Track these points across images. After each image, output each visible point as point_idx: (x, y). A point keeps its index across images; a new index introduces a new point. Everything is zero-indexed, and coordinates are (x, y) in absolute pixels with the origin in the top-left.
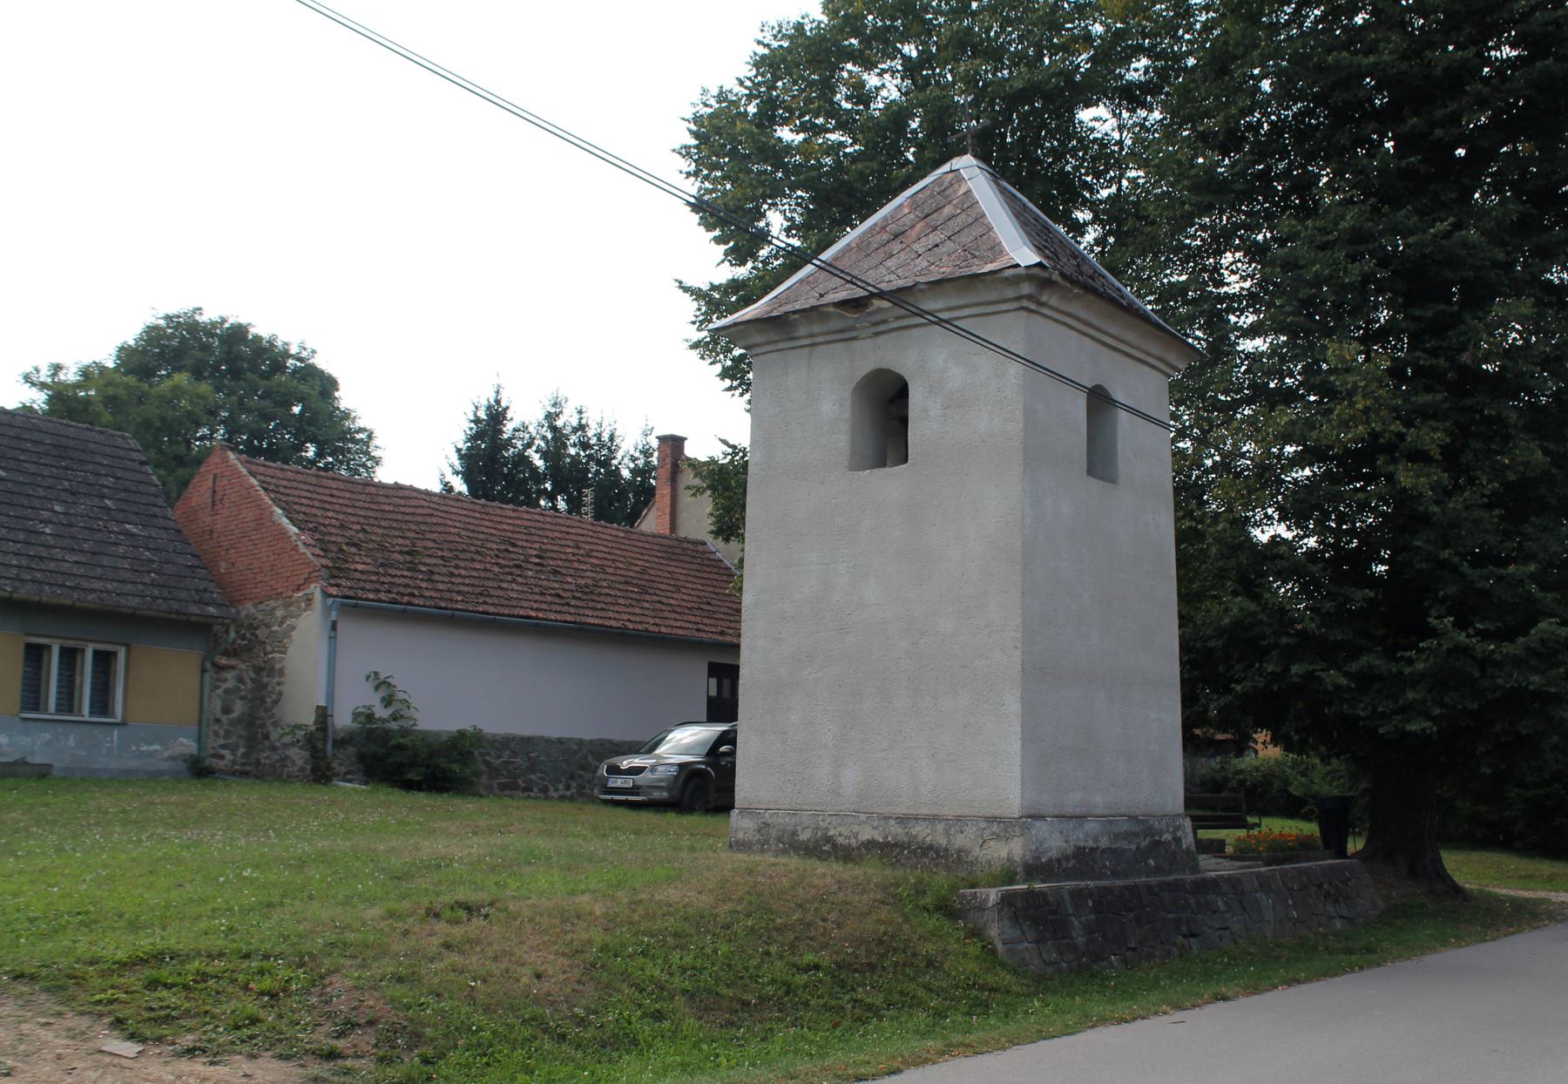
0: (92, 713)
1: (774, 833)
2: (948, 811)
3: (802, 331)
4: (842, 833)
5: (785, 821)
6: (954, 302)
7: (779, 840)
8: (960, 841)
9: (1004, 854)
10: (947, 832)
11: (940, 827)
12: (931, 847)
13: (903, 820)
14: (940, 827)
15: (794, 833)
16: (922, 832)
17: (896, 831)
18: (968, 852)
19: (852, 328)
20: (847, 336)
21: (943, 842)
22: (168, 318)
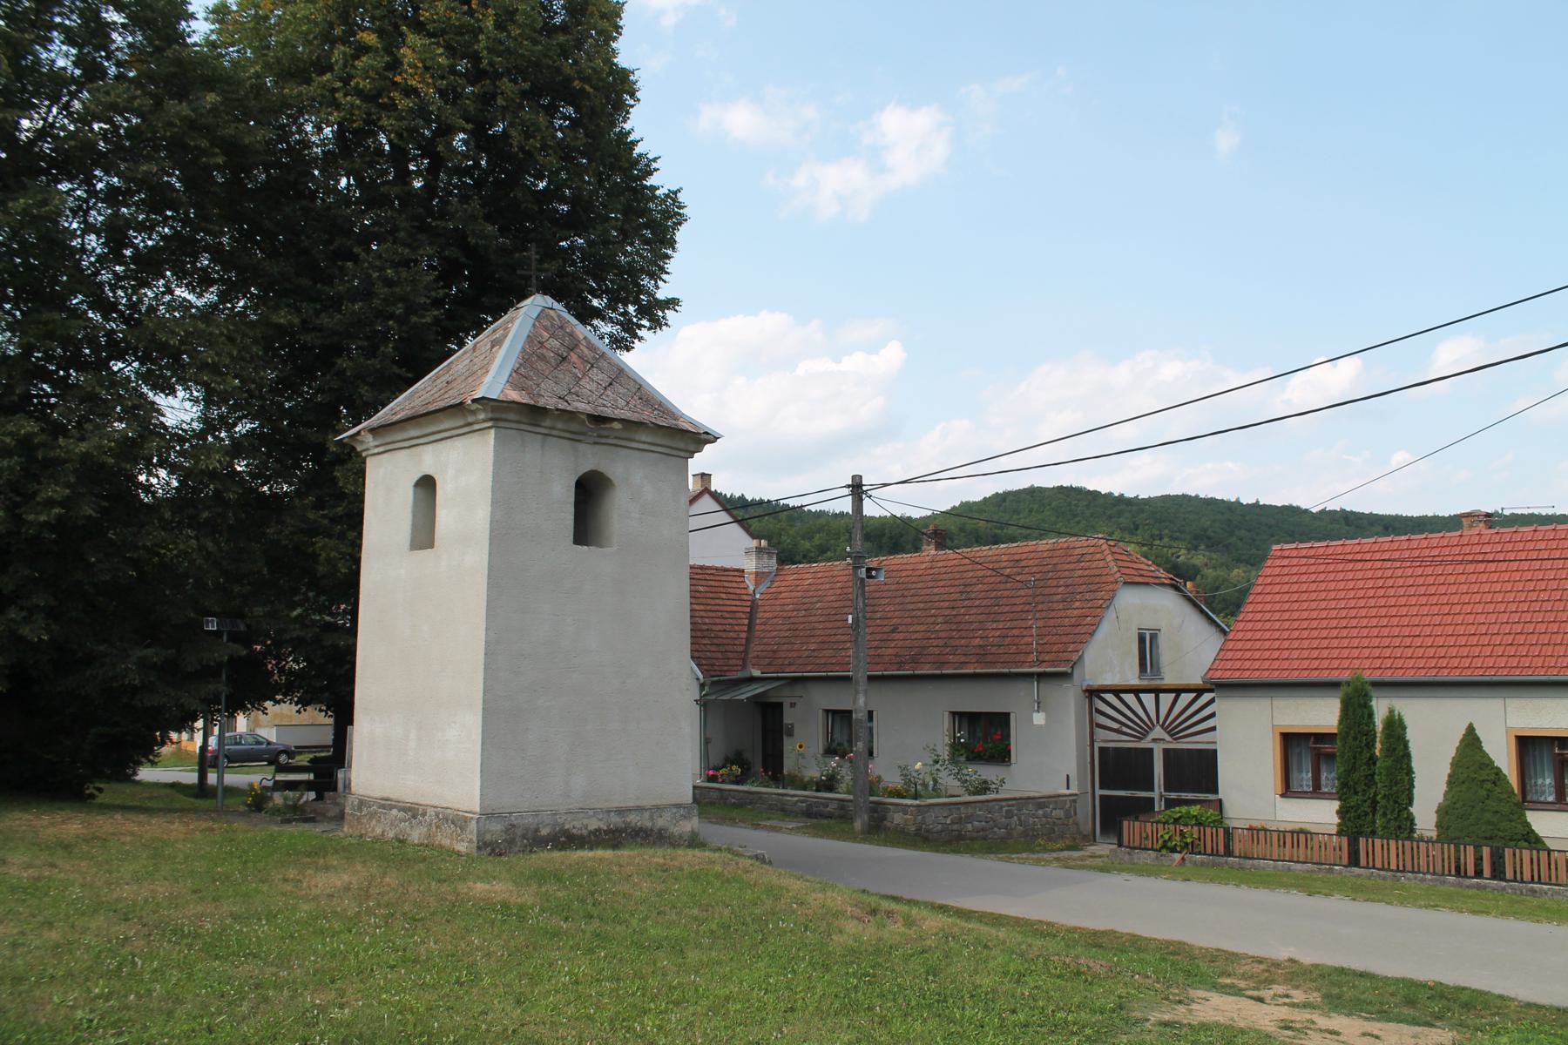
0: (1151, 750)
1: (519, 832)
2: (646, 803)
3: (548, 423)
4: (575, 825)
5: (530, 821)
6: (658, 441)
7: (524, 837)
8: (660, 823)
9: (689, 829)
10: (651, 818)
11: (647, 815)
12: (641, 829)
13: (621, 811)
14: (647, 815)
15: (537, 830)
16: (634, 819)
17: (616, 820)
18: (666, 830)
19: (584, 434)
20: (575, 437)
21: (649, 825)
22: (673, 195)
